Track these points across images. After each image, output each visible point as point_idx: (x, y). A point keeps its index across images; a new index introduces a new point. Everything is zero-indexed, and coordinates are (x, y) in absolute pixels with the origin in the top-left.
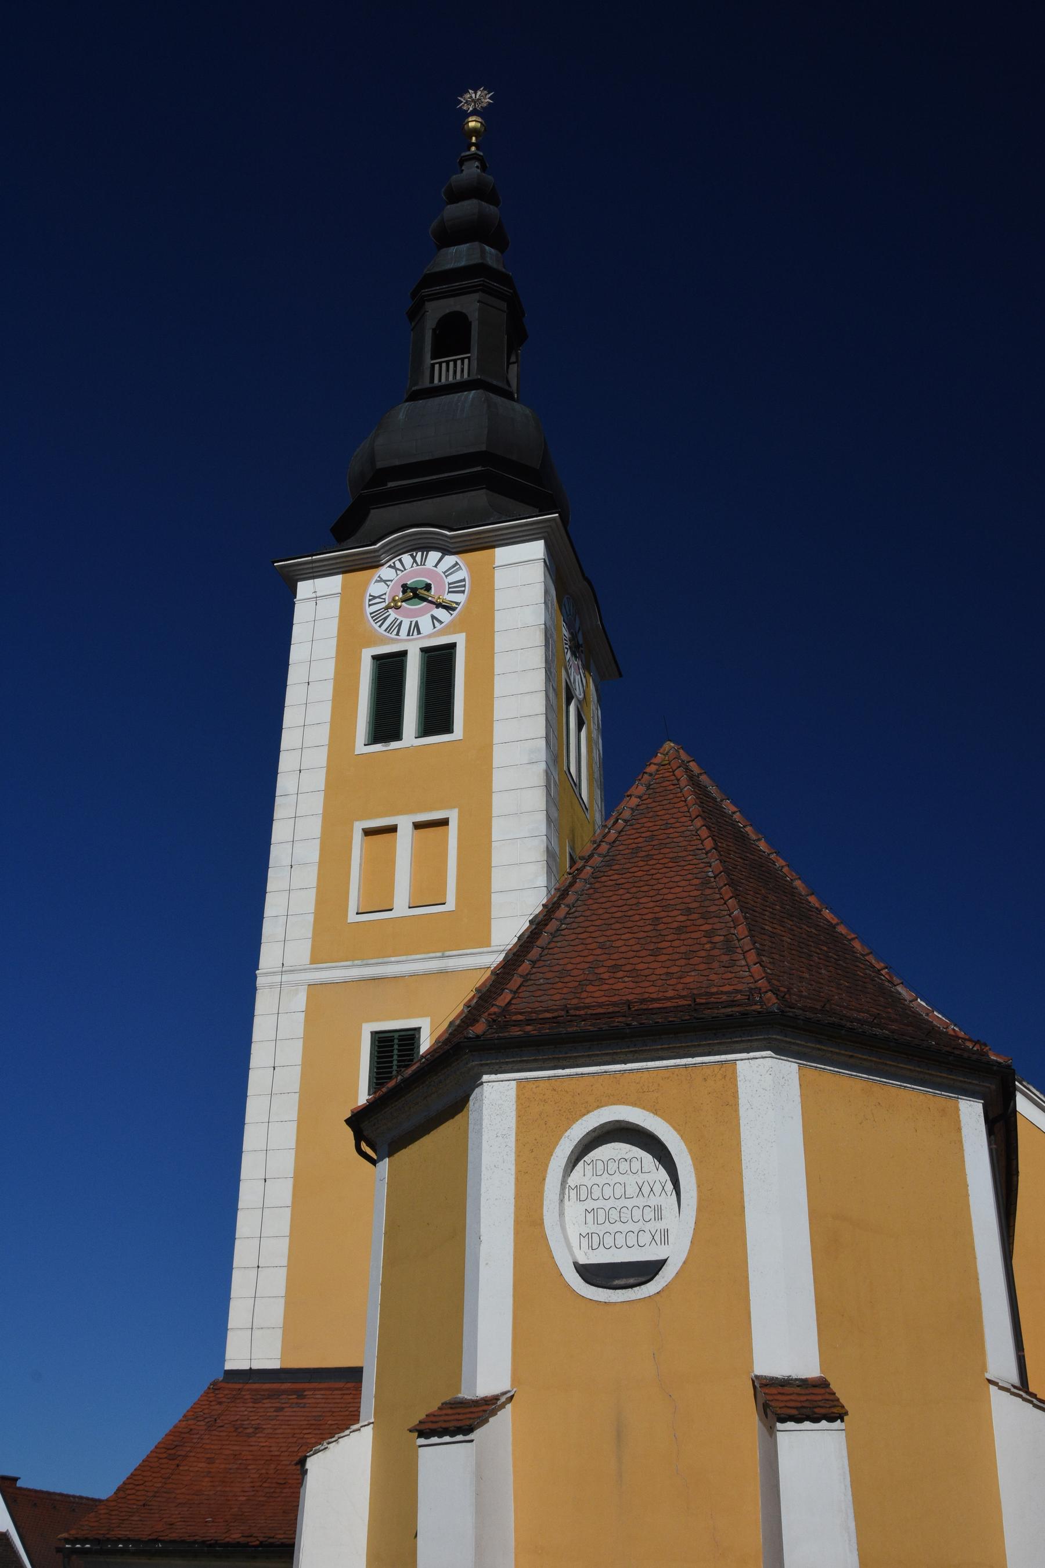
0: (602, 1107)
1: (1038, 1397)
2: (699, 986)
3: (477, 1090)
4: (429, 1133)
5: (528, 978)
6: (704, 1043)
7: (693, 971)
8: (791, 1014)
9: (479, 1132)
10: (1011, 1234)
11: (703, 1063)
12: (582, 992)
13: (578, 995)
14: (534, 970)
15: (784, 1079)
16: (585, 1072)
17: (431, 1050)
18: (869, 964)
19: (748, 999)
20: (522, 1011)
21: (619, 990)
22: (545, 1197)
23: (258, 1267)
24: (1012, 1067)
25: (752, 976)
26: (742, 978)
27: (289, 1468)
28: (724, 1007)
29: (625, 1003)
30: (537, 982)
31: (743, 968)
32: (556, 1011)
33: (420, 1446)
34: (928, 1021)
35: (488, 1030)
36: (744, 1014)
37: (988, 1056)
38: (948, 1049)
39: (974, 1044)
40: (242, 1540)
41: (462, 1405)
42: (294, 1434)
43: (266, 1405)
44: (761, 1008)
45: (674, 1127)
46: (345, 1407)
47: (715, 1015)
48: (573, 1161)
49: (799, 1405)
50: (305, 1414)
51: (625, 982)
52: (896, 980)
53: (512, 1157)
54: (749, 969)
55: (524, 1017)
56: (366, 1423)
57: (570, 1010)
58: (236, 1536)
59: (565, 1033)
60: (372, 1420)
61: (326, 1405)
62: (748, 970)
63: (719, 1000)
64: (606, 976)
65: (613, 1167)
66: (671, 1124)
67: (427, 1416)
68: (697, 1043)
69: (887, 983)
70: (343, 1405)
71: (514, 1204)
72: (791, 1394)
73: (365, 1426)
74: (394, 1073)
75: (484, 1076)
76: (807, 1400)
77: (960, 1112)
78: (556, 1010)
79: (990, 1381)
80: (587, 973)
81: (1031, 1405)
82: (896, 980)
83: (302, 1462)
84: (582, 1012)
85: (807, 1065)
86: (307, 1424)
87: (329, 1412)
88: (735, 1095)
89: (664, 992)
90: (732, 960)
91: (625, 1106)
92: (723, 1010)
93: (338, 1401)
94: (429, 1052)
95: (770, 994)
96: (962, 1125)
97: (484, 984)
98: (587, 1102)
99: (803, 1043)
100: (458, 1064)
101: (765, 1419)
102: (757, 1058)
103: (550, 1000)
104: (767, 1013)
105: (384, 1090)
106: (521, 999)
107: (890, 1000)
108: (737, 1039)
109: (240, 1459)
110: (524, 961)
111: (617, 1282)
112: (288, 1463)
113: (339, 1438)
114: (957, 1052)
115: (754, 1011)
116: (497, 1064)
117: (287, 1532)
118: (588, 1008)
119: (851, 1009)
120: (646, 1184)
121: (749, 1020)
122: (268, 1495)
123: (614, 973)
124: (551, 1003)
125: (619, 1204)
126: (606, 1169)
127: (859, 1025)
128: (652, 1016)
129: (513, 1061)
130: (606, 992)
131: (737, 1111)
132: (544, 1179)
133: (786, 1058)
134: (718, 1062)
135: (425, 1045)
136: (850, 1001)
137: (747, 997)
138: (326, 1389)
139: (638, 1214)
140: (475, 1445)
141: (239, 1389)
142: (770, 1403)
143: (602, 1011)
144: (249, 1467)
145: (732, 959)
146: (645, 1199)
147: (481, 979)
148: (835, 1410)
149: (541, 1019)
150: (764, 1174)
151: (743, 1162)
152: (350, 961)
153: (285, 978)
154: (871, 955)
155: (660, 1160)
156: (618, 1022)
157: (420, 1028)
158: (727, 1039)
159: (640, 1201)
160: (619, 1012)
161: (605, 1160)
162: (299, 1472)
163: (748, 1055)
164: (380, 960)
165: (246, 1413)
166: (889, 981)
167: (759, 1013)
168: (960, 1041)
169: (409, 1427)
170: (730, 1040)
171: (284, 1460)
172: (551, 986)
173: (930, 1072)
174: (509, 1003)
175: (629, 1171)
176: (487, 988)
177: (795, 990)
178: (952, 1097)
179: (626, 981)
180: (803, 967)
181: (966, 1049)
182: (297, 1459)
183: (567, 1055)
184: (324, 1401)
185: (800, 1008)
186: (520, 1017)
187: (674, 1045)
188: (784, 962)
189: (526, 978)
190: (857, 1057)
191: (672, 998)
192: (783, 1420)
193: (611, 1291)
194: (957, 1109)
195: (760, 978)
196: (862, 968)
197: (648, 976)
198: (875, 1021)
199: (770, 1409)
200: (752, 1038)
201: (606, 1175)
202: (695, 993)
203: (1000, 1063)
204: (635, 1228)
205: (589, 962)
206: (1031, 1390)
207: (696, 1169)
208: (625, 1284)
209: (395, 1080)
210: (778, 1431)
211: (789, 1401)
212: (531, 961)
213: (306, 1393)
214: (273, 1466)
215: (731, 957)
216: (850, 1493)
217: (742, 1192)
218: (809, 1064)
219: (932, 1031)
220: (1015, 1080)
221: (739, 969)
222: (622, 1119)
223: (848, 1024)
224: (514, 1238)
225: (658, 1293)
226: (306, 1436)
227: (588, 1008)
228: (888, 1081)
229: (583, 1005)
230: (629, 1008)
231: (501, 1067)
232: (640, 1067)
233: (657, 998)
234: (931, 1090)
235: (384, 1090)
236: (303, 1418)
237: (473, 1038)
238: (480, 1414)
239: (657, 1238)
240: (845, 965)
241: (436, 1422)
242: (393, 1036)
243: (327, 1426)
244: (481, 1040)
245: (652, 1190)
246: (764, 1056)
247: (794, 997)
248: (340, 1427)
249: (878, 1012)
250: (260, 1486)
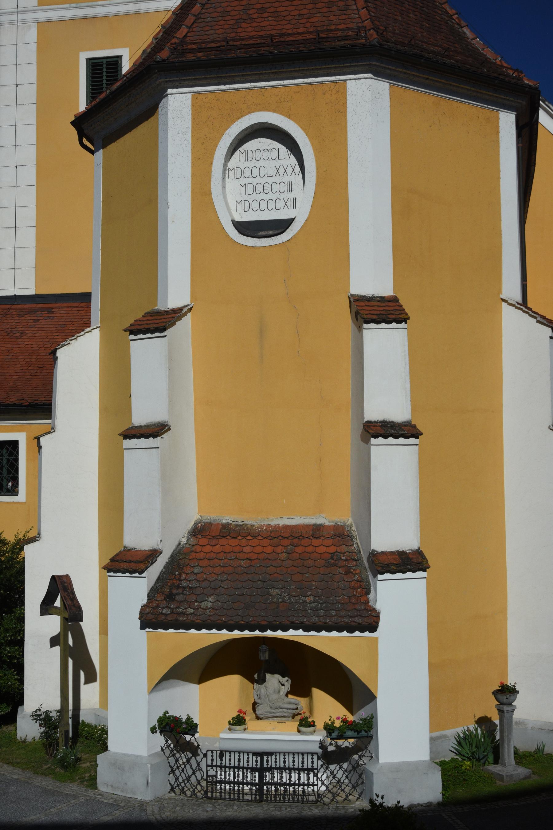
0: (252, 112)
1: (533, 310)
2: (322, 24)
3: (164, 100)
4: (130, 131)
5: (199, 17)
6: (324, 67)
7: (318, 13)
8: (386, 47)
9: (166, 131)
10: (525, 218)
11: (323, 82)
12: (238, 28)
13: (235, 30)
14: (204, 11)
15: (379, 94)
16: (240, 87)
17: (130, 71)
18: (444, 10)
19: (357, 35)
20: (195, 41)
21: (264, 27)
22: (212, 176)
23: (16, 227)
24: (539, 89)
25: (360, 18)
26: (353, 19)
27: (45, 357)
28: (339, 41)
29: (268, 37)
30: (206, 20)
31: (354, 12)
32: (220, 42)
33: (131, 340)
34: (483, 54)
35: (171, 55)
36: (353, 46)
37: (523, 81)
38: (495, 75)
39: (514, 71)
40: (17, 402)
41: (158, 314)
42: (48, 336)
43: (28, 318)
44: (365, 42)
45: (301, 127)
46: (81, 318)
47: (332, 46)
48: (231, 151)
49: (378, 313)
50: (54, 323)
51: (269, 21)
52: (463, 23)
53: (189, 148)
54: (358, 12)
55: (197, 46)
56: (95, 327)
57: (230, 41)
58: (13, 400)
59: (226, 59)
60: (99, 325)
61: (68, 317)
62: (357, 13)
63: (335, 35)
64: (255, 16)
65: (259, 155)
66: (299, 125)
67: (135, 321)
68: (319, 67)
69: (456, 26)
70: (80, 317)
71: (191, 181)
72: (373, 306)
73: (95, 329)
74: (104, 89)
75: (168, 90)
76: (384, 310)
77: (500, 120)
78: (219, 41)
79: (503, 300)
80: (242, 13)
81: (528, 315)
82: (463, 23)
83: (54, 352)
84: (238, 43)
85: (395, 84)
86: (56, 330)
87: (70, 321)
88: (345, 105)
89: (297, 29)
90: (346, 5)
91: (268, 112)
92: (338, 43)
93: (75, 315)
94: (128, 73)
95: (372, 31)
96: (500, 129)
97: (167, 21)
98: (241, 109)
99: (394, 68)
100: (150, 81)
101: (356, 321)
102: (361, 79)
103: (215, 33)
104: (370, 45)
105: (98, 100)
106: (195, 33)
107: (457, 38)
108: (348, 65)
109: (12, 353)
110: (196, 4)
111: (261, 234)
112: (44, 354)
113: (77, 337)
114: (501, 77)
115: (360, 44)
116: (177, 81)
117: (46, 397)
118: (242, 40)
119: (429, 44)
120: (281, 167)
121: (357, 50)
122: (33, 374)
123: (261, 13)
124: (215, 36)
125: (263, 181)
126: (254, 156)
127: (434, 56)
128: (288, 46)
129: (189, 79)
130: (255, 28)
131: (345, 116)
132: (212, 163)
133: (381, 79)
134: (334, 81)
135: (126, 67)
136: (429, 38)
137: (356, 33)
138: (69, 307)
139: (275, 187)
140: (167, 340)
141: (8, 309)
142: (360, 312)
143: (251, 42)
144: (19, 358)
145: (346, 4)
146: (281, 177)
147: (164, 18)
148: (402, 316)
149: (209, 48)
150: (363, 161)
151: (348, 152)
152: (68, 4)
153: (20, 17)
154: (446, 4)
155: (292, 150)
156: (264, 51)
157: (122, 56)
158: (340, 64)
159: (278, 179)
160: (264, 43)
161: (254, 150)
162: (52, 360)
163: (355, 76)
164: (90, 4)
165: (14, 323)
166: (458, 24)
167: (364, 45)
168: (504, 69)
169: (123, 329)
170: (342, 65)
171: (42, 353)
172: (216, 23)
173: (481, 91)
174: (186, 36)
175: (270, 158)
176: (169, 25)
177: (391, 28)
178: (495, 110)
179: (270, 20)
180: (397, 12)
181: (508, 75)
182: (50, 351)
183: (227, 75)
184: (66, 315)
185: (393, 43)
186: (194, 46)
187: (303, 68)
188: (384, 7)
189: (198, 17)
190: (431, 79)
191: (303, 33)
192: (367, 322)
193: (257, 239)
194: (498, 118)
195: (366, 18)
196: (439, 13)
197: (286, 16)
198: (446, 53)
199: (360, 316)
200: (358, 64)
201: (254, 160)
202: (319, 29)
203: (530, 86)
204: (274, 197)
205: (244, 5)
206: (529, 305)
207: (316, 157)
208: (267, 234)
209: (105, 93)
210: (364, 329)
211: (372, 310)
212: (202, 4)
213: (53, 310)
214: (34, 357)
215: (346, 3)
216: (408, 367)
217: (347, 173)
218: (397, 83)
219: (485, 61)
220: (539, 100)
221: (351, 12)
222: (265, 121)
223: (426, 55)
224: (192, 203)
225: (288, 240)
226: (55, 337)
227: (242, 40)
228: (451, 97)
229: (238, 37)
230: (272, 41)
231: (181, 83)
232: (279, 84)
233: (292, 33)
234: (480, 104)
235: (98, 100)
236: (53, 326)
237: (160, 62)
238: (171, 319)
239: (289, 204)
240: (427, 11)
241: (141, 325)
242: (103, 62)
243: (69, 331)
244: (166, 63)
245: (285, 171)
246: (366, 77)
247: (390, 34)
248: (77, 331)
249: (449, 46)
250: (27, 369)
